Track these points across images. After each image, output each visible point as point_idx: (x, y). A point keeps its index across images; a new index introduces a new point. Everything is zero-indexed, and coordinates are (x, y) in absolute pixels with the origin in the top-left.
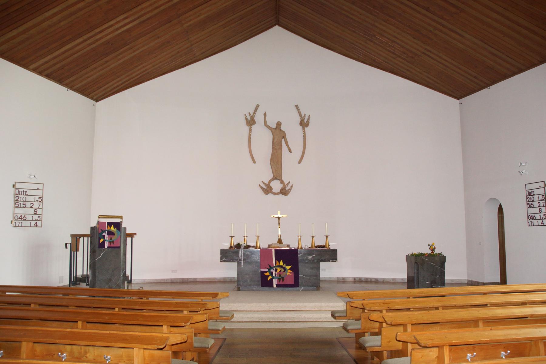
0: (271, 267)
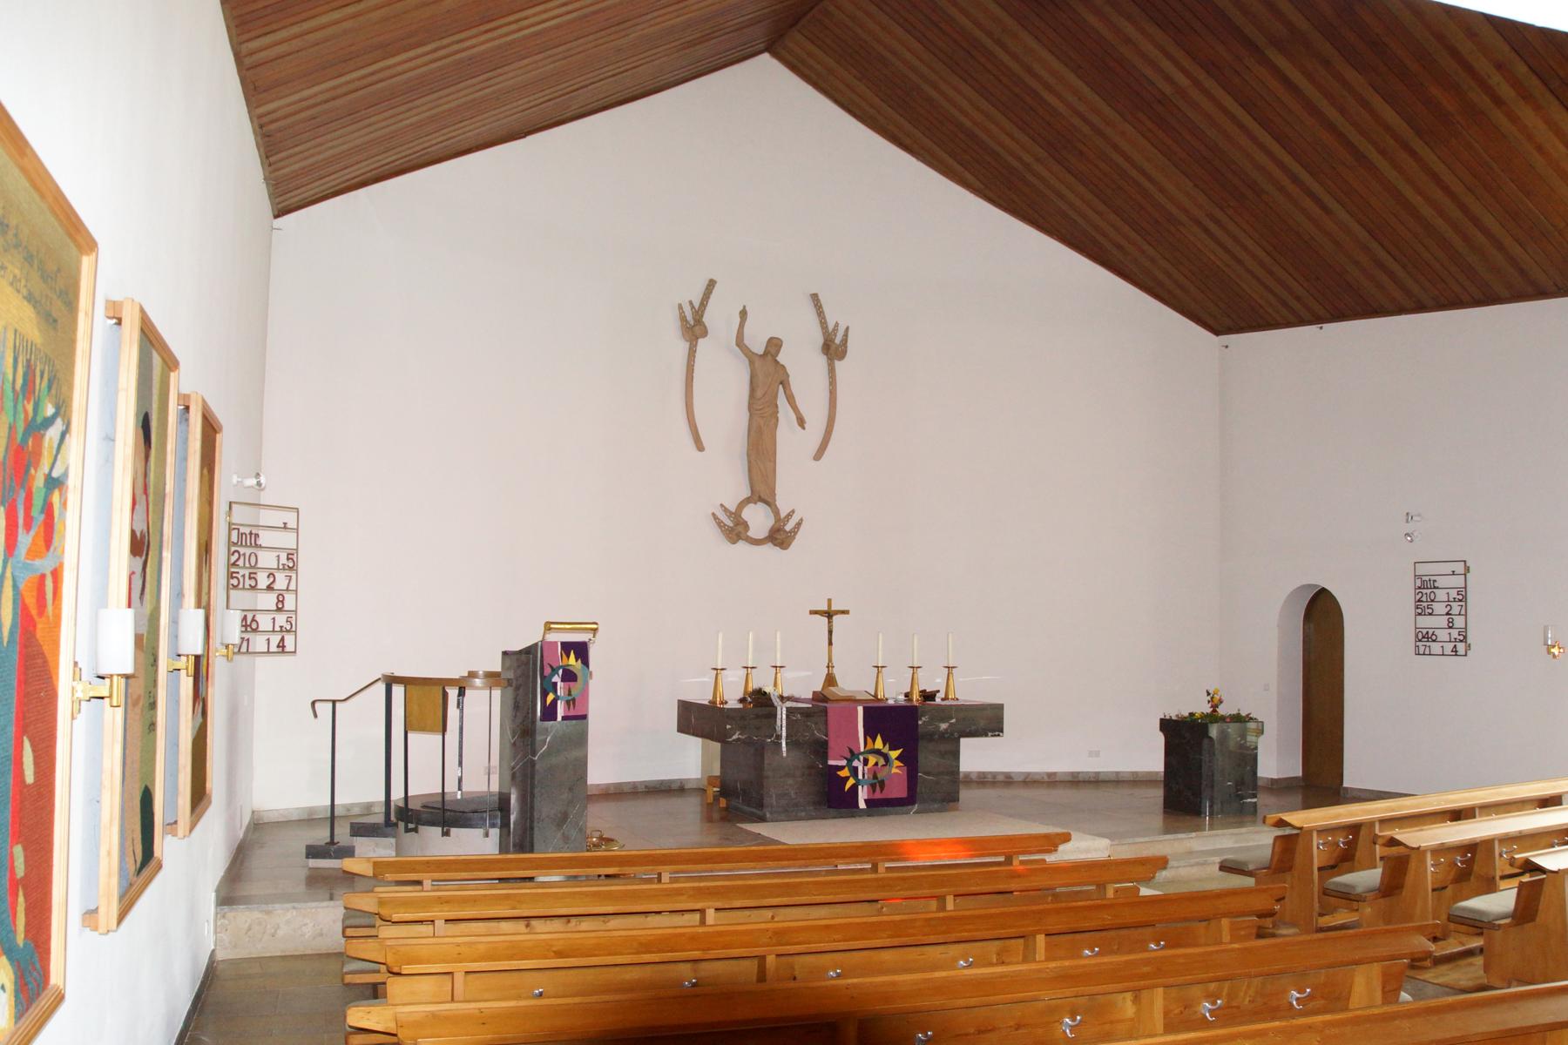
0: (853, 755)
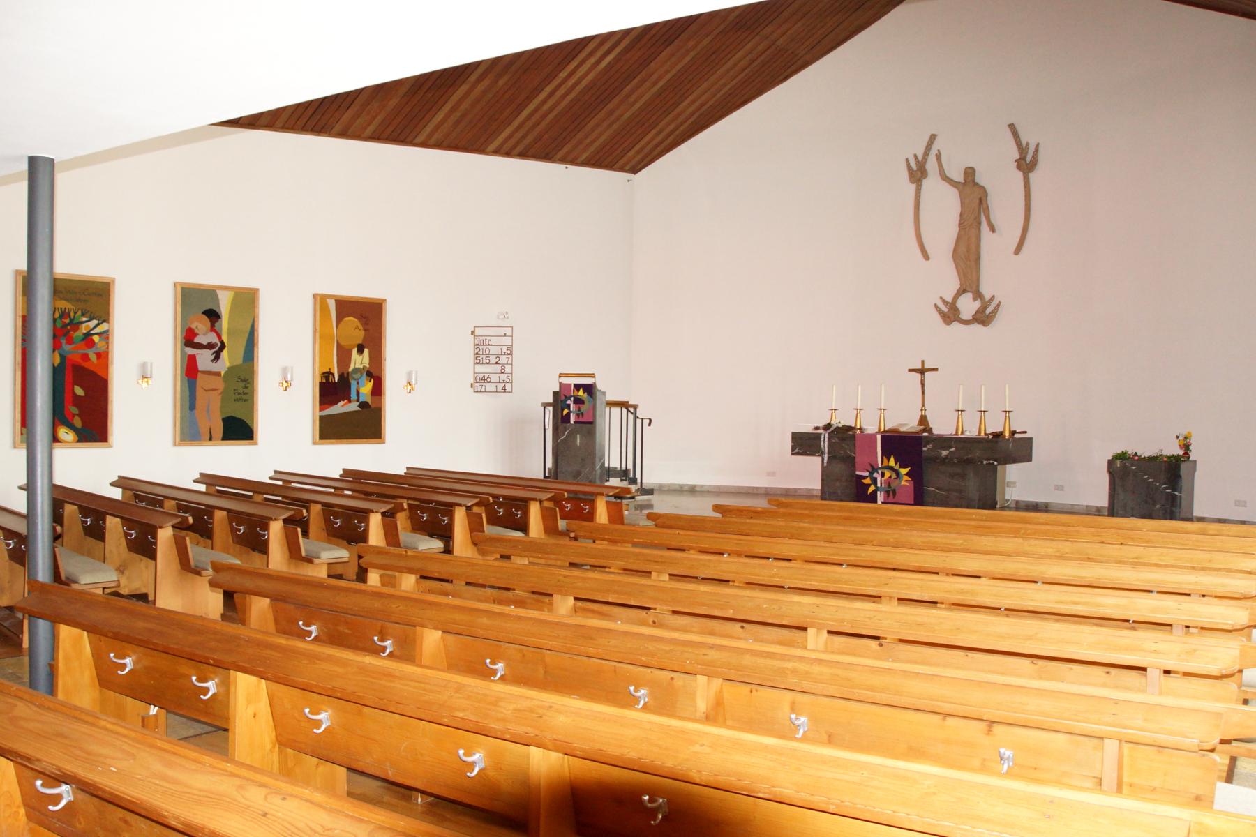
0: (874, 469)
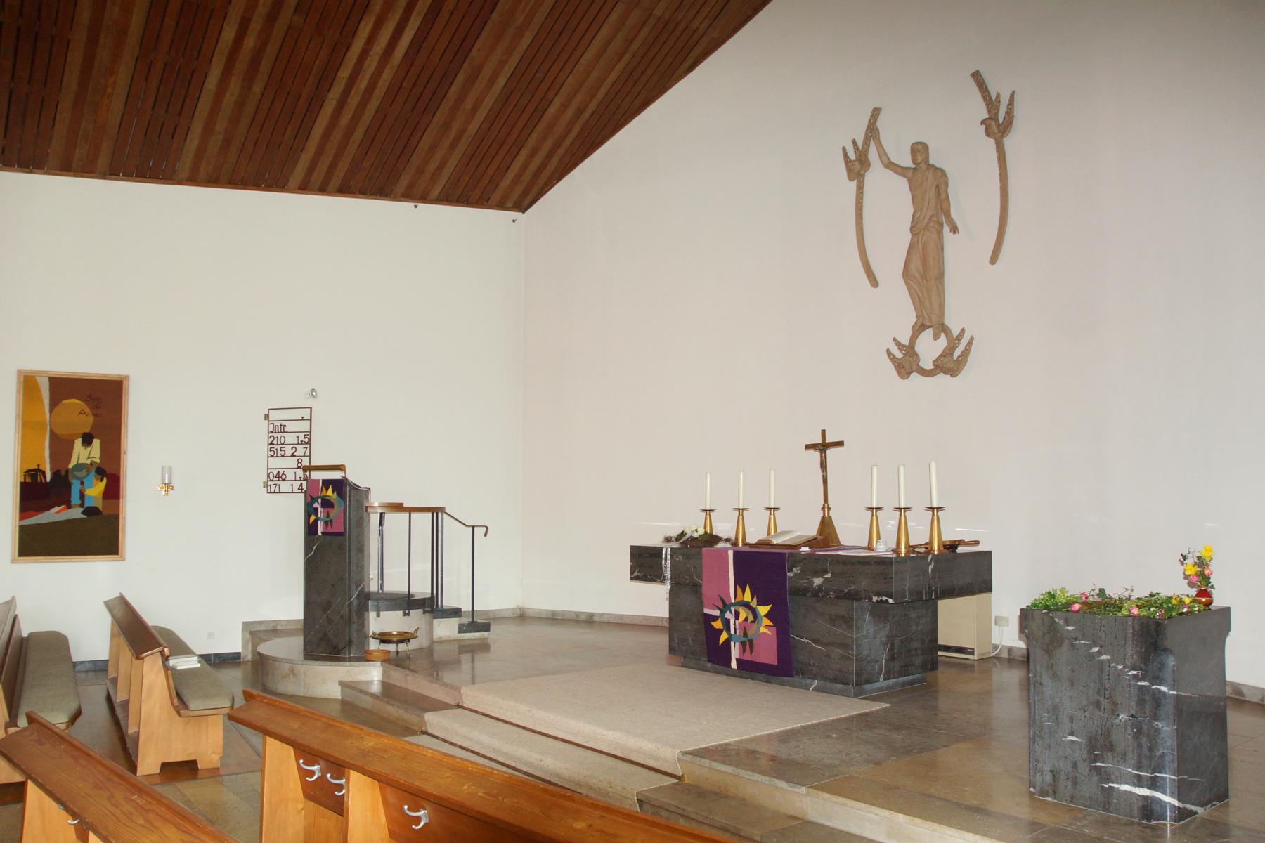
0: (725, 606)
